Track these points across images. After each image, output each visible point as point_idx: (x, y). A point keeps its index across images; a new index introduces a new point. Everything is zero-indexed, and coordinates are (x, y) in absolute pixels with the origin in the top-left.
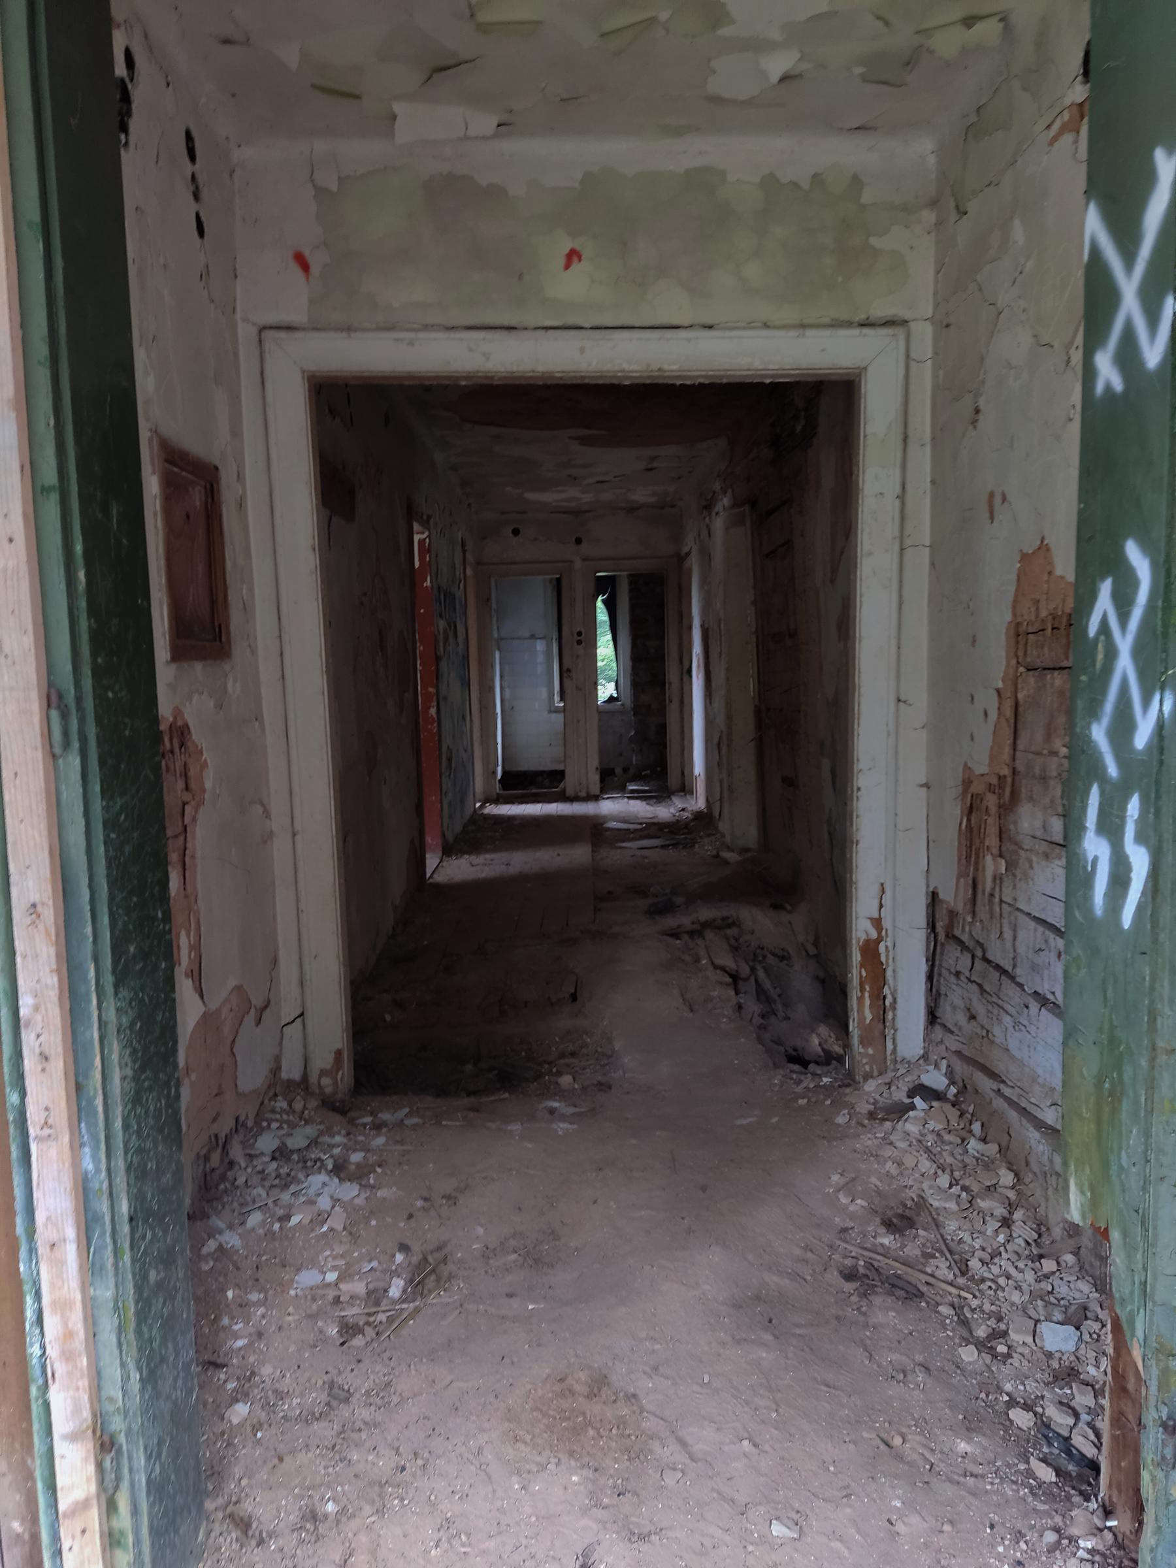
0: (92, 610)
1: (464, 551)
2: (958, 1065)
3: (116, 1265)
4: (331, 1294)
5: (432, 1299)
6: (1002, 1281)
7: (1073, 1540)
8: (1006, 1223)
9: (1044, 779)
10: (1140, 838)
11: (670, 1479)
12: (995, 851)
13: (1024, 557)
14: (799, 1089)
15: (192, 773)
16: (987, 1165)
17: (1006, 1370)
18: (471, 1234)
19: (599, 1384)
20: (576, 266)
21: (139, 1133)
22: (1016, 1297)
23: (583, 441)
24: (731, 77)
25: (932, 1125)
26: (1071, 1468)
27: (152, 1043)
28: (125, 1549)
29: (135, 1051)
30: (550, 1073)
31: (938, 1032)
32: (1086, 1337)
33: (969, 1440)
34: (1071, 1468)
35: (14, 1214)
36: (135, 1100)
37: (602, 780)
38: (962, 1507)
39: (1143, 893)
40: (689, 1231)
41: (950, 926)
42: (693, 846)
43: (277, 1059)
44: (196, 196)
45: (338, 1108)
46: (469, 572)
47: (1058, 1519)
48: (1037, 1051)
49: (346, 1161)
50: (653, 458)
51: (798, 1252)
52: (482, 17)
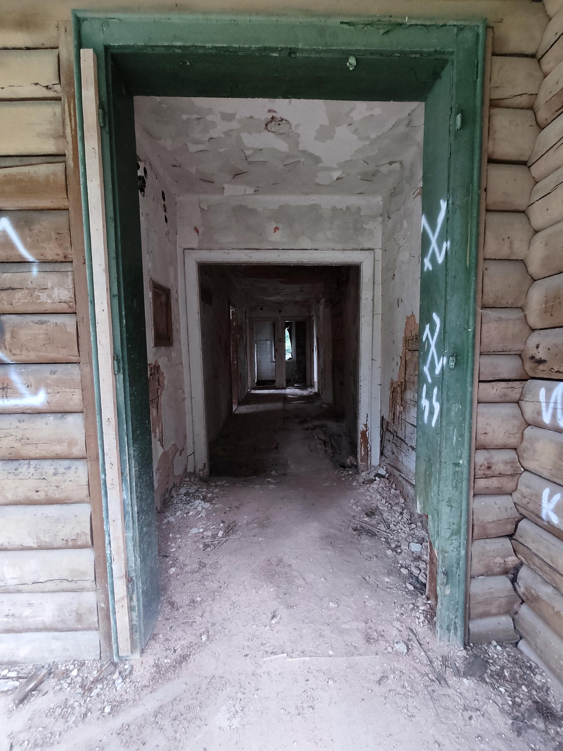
0: (127, 332)
2: (389, 467)
3: (133, 526)
4: (201, 535)
5: (230, 537)
6: (400, 531)
7: (418, 607)
8: (401, 513)
9: (413, 383)
10: (437, 400)
11: (300, 590)
12: (400, 404)
13: (407, 318)
14: (342, 475)
15: (161, 380)
16: (397, 497)
17: (400, 557)
18: (243, 518)
19: (280, 561)
20: (277, 231)
21: (140, 487)
22: (403, 535)
23: (282, 282)
24: (322, 178)
25: (381, 485)
26: (418, 586)
27: (144, 460)
28: (135, 612)
29: (139, 463)
30: (269, 470)
31: (383, 458)
32: (424, 547)
33: (389, 578)
34: (418, 586)
35: (102, 511)
36: (139, 477)
37: (287, 383)
38: (386, 598)
39: (438, 416)
40: (308, 517)
41: (387, 426)
43: (186, 466)
44: (165, 211)
45: (205, 481)
47: (414, 601)
48: (409, 462)
49: (206, 496)
50: (302, 288)
51: (340, 523)
52: (249, 160)
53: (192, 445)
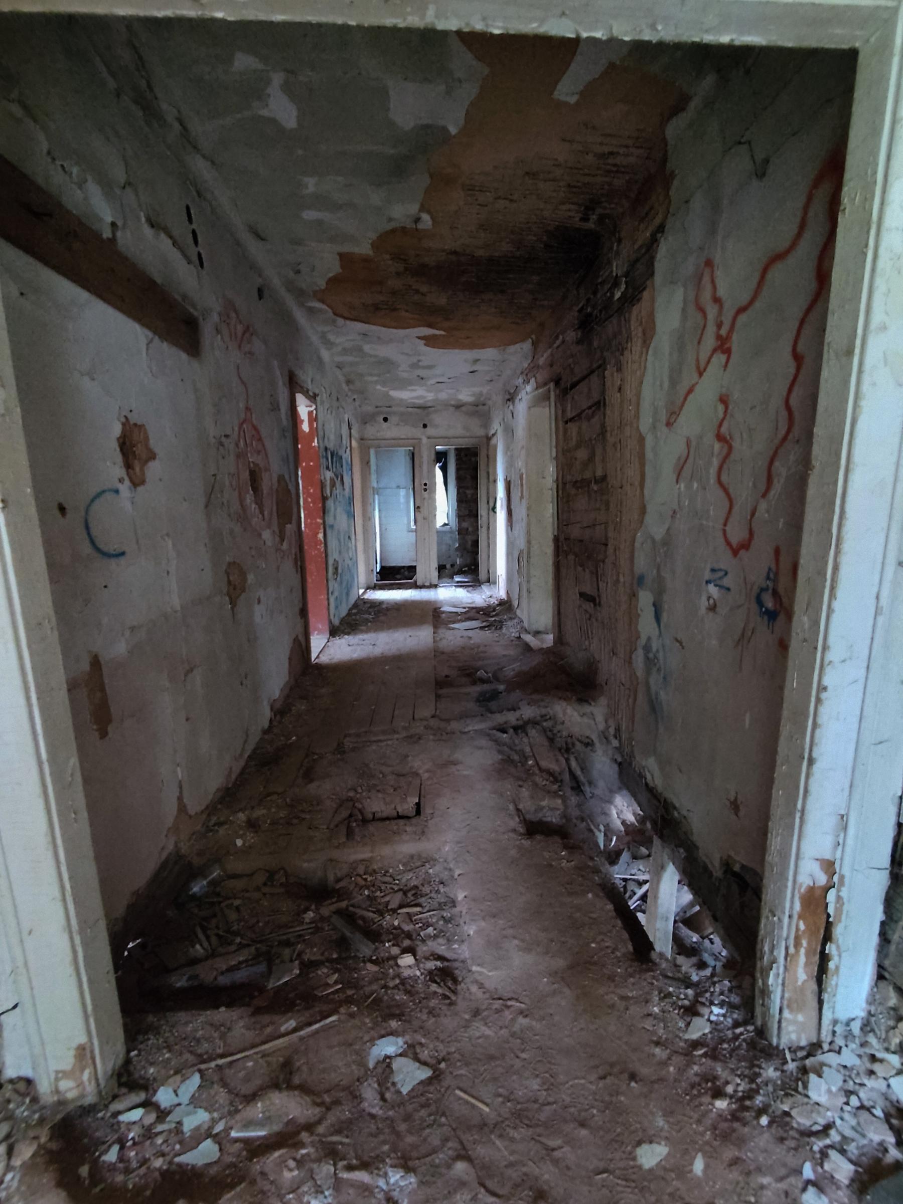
1: (350, 429)
23: (430, 341)
42: (501, 628)
46: (354, 443)
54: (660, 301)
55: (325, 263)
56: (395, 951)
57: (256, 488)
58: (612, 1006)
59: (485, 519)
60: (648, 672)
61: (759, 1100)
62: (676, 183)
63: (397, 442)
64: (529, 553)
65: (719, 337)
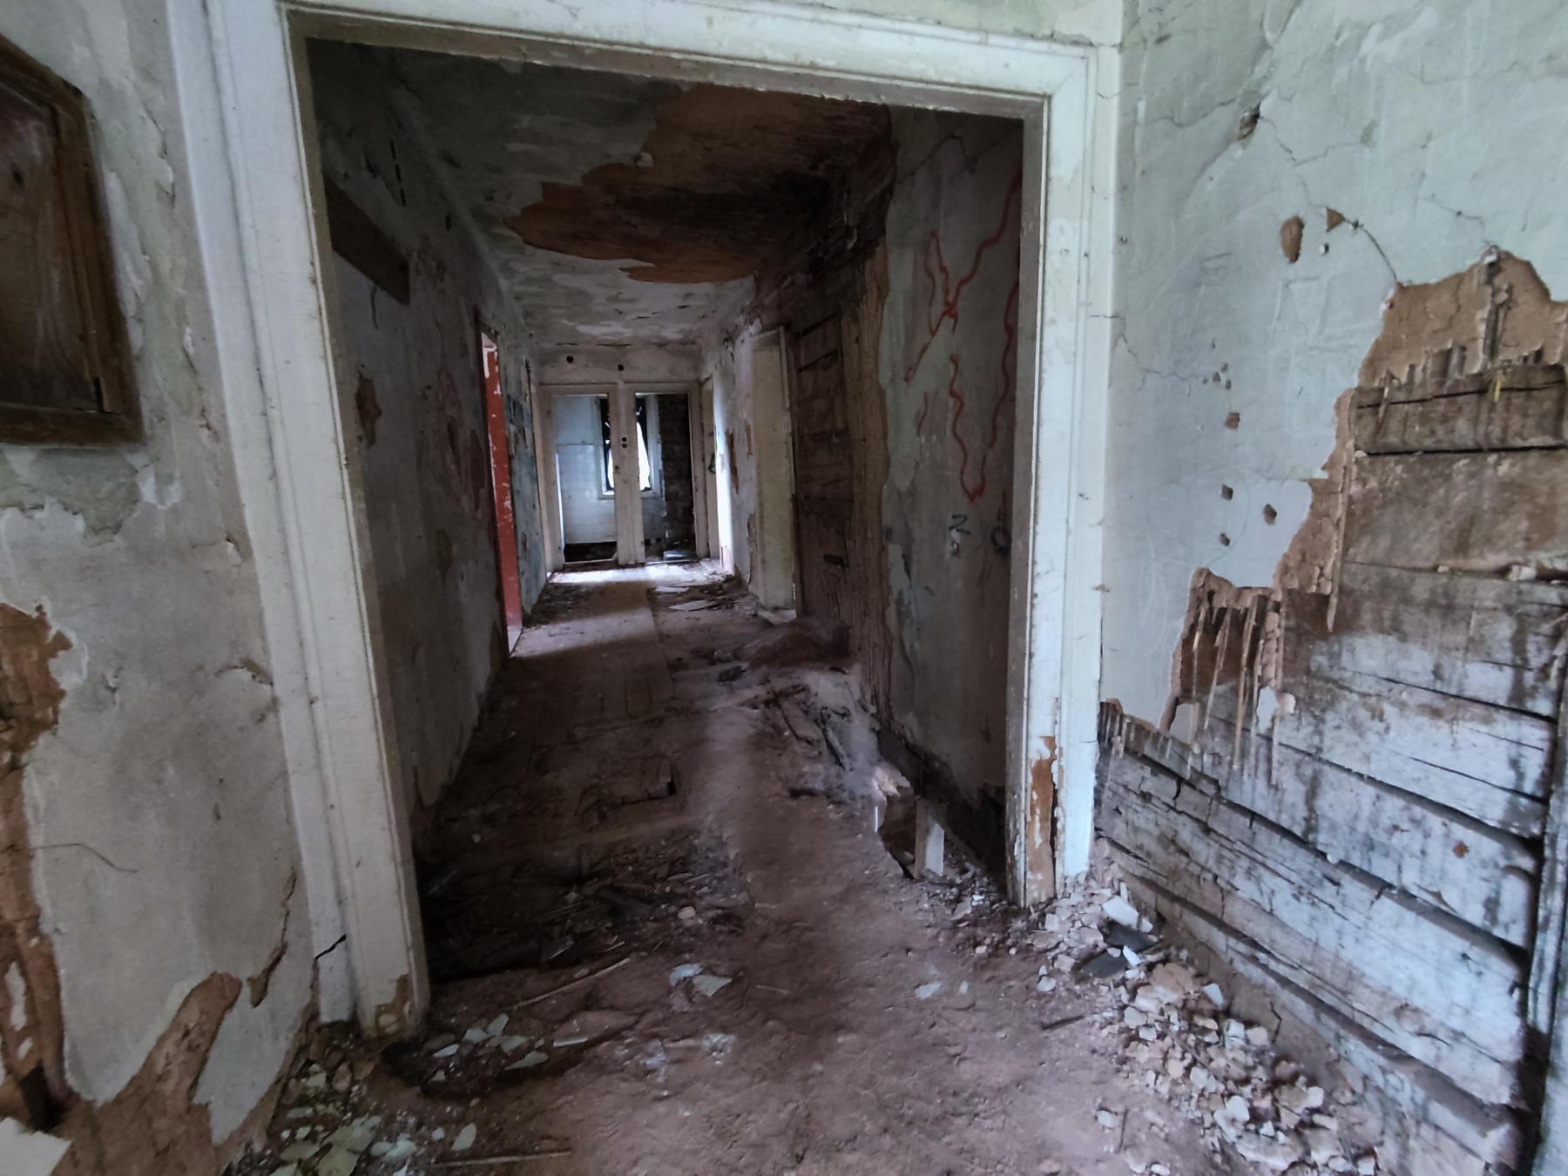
23: (634, 273)
50: (688, 295)
53: (331, 910)
54: (893, 260)
55: (526, 190)
56: (673, 909)
57: (454, 446)
58: (889, 910)
59: (700, 479)
60: (901, 623)
61: (1009, 942)
62: (900, 153)
63: (583, 387)
64: (762, 517)
65: (946, 303)
